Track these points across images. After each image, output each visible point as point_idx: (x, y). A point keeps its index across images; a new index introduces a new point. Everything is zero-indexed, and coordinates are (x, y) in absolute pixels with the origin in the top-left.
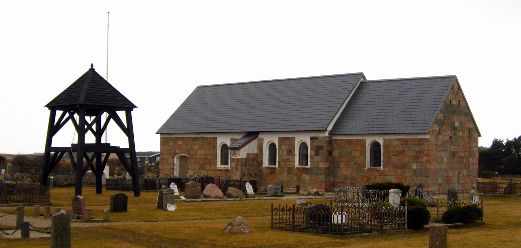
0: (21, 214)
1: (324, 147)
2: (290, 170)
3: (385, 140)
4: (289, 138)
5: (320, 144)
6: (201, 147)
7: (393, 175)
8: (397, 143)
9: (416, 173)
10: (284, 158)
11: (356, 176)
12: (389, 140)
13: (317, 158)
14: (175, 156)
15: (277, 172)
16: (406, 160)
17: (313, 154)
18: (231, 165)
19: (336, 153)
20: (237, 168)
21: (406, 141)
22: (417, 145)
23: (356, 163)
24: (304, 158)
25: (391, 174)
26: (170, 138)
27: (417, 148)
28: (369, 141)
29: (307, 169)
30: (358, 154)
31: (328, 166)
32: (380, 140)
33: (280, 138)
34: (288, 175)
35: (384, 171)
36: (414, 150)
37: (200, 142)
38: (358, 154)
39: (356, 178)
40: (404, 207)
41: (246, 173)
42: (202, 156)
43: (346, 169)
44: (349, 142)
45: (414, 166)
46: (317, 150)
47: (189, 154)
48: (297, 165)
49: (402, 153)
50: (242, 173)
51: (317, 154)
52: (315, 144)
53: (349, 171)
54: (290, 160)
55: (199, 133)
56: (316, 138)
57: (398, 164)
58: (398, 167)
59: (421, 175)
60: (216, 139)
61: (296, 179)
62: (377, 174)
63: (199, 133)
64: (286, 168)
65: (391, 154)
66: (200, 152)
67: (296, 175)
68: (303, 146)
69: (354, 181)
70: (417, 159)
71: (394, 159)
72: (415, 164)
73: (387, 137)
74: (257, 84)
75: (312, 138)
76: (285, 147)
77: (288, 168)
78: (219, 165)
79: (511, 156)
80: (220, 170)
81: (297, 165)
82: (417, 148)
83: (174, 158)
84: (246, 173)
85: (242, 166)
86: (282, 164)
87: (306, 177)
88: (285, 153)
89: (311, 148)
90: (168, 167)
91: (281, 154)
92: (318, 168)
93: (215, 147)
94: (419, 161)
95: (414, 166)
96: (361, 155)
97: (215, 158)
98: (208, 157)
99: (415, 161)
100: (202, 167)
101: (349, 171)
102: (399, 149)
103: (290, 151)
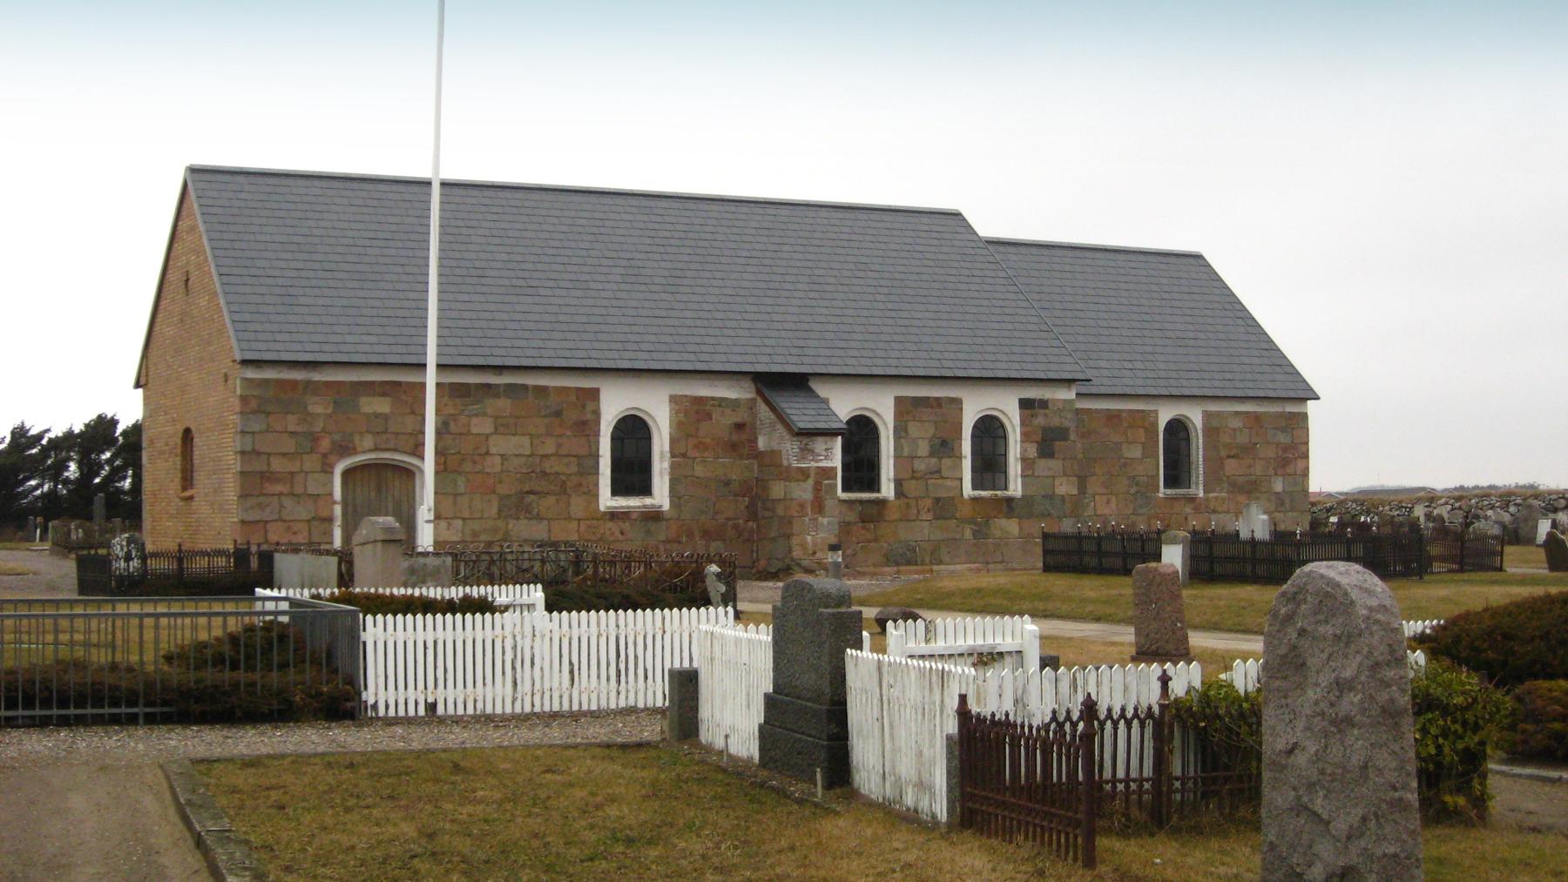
2: (944, 508)
3: (1207, 416)
4: (937, 399)
5: (1056, 422)
6: (503, 427)
7: (1228, 512)
8: (1236, 423)
9: (1282, 504)
10: (920, 466)
11: (1133, 518)
12: (1219, 414)
13: (1044, 466)
15: (892, 514)
16: (1258, 470)
17: (1032, 451)
21: (1257, 417)
22: (1283, 430)
23: (1133, 479)
24: (989, 465)
26: (309, 383)
27: (1284, 439)
28: (1165, 414)
30: (1136, 452)
32: (1195, 415)
34: (940, 522)
35: (1208, 500)
36: (1278, 444)
37: (503, 404)
38: (1136, 452)
40: (320, 670)
44: (1112, 417)
46: (1046, 442)
48: (968, 490)
49: (1247, 450)
51: (1046, 451)
52: (1040, 421)
53: (1113, 504)
55: (499, 369)
56: (1044, 404)
57: (1241, 479)
59: (1293, 509)
60: (594, 394)
61: (968, 534)
62: (1188, 510)
63: (499, 369)
64: (928, 502)
65: (1223, 453)
66: (499, 445)
67: (972, 521)
70: (1284, 466)
71: (1231, 467)
73: (1213, 407)
74: (798, 212)
75: (1025, 404)
76: (923, 434)
77: (938, 500)
78: (607, 500)
80: (613, 515)
81: (968, 490)
82: (1284, 439)
86: (911, 487)
88: (923, 449)
90: (303, 512)
91: (906, 453)
93: (588, 427)
95: (1278, 486)
96: (1145, 456)
98: (552, 466)
99: (1280, 471)
101: (1113, 504)
102: (1242, 439)
103: (944, 443)
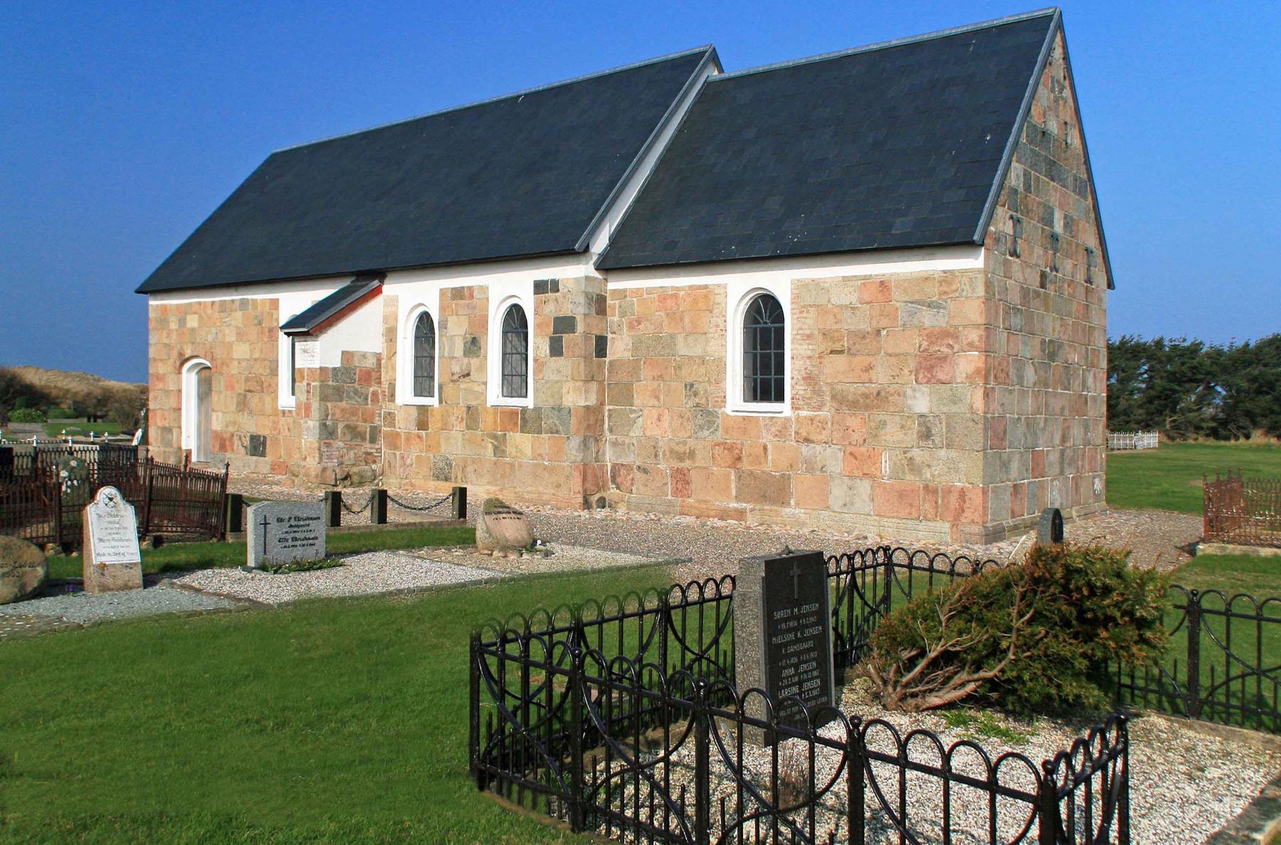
0: (829, 576)
1: (579, 319)
5: (566, 310)
14: (182, 364)
16: (881, 376)
18: (536, 397)
19: (619, 348)
20: (308, 408)
25: (824, 436)
29: (524, 409)
31: (592, 401)
33: (443, 292)
39: (692, 454)
41: (341, 426)
42: (244, 364)
43: (655, 413)
45: (921, 402)
47: (213, 360)
50: (324, 426)
51: (556, 349)
54: (474, 376)
56: (554, 286)
58: (854, 405)
68: (515, 320)
69: (687, 464)
72: (925, 389)
75: (540, 287)
79: (1042, 373)
82: (928, 319)
83: (180, 373)
84: (341, 426)
85: (324, 398)
87: (521, 442)
89: (537, 326)
92: (558, 409)
94: (941, 376)
95: (921, 402)
97: (274, 372)
100: (243, 405)
101: (665, 423)
103: (474, 341)
